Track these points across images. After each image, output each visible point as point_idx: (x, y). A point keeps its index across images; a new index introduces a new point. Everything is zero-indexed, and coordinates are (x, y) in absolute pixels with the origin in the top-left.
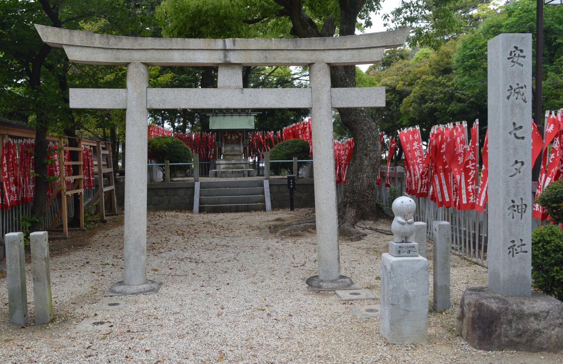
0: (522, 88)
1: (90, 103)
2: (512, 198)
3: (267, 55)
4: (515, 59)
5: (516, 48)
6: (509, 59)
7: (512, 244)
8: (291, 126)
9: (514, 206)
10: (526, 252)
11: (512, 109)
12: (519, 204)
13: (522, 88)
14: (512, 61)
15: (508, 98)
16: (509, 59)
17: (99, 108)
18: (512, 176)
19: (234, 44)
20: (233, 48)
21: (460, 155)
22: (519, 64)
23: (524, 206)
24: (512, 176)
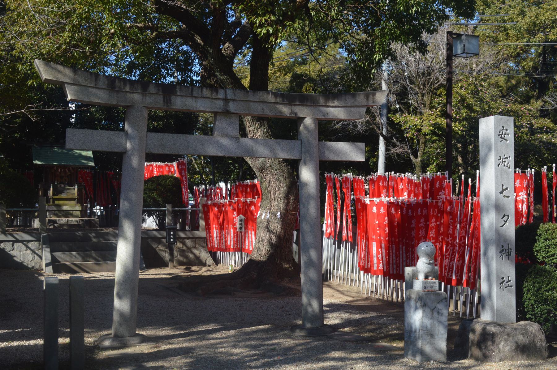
0: (507, 158)
1: (89, 144)
2: (502, 244)
3: (264, 107)
4: (503, 136)
5: (503, 127)
6: (499, 135)
7: (502, 280)
8: (196, 166)
9: (503, 250)
10: (511, 286)
11: (501, 175)
12: (507, 248)
13: (507, 158)
14: (501, 138)
15: (498, 165)
16: (499, 135)
17: (97, 150)
18: (502, 226)
19: (235, 96)
20: (233, 98)
21: (65, 186)
22: (505, 139)
23: (510, 250)
24: (502, 226)
